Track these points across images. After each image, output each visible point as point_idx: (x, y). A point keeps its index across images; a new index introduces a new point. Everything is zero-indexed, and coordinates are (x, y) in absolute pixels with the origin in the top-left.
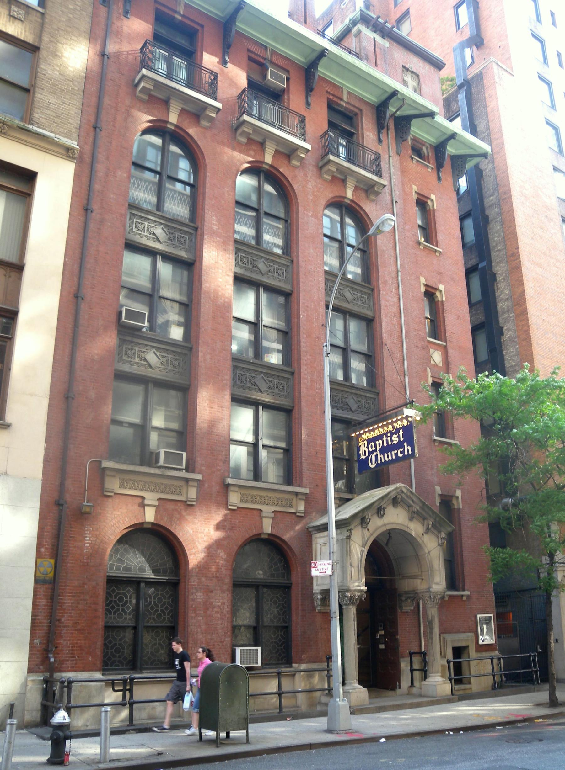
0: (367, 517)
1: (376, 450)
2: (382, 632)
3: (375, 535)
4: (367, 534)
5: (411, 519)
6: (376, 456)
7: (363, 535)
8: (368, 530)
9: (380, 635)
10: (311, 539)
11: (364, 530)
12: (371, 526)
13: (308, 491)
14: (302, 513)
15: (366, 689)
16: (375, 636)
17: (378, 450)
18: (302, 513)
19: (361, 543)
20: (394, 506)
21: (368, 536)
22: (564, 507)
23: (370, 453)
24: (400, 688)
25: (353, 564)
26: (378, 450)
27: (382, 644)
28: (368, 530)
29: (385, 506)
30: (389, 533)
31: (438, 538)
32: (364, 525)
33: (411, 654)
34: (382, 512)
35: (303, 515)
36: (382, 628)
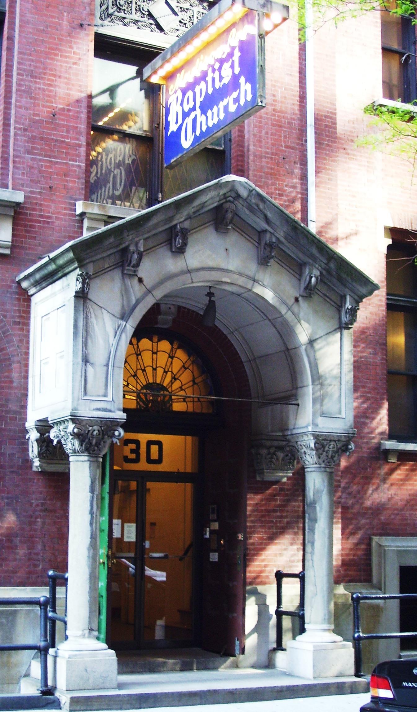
0: (132, 248)
1: (194, 109)
2: (215, 526)
3: (159, 294)
4: (136, 290)
5: (263, 262)
6: (195, 120)
7: (125, 292)
8: (140, 280)
9: (211, 532)
10: (29, 306)
11: (128, 282)
12: (149, 269)
13: (19, 197)
14: (6, 247)
15: (112, 652)
16: (203, 533)
17: (198, 105)
18: (6, 247)
19: (117, 310)
20: (217, 230)
21: (139, 295)
22: (118, 1)
23: (186, 115)
24: (243, 651)
25: (91, 359)
26: (198, 105)
27: (215, 551)
28: (140, 280)
29: (187, 225)
30: (210, 294)
31: (339, 312)
32: (129, 269)
33: (280, 576)
34: (179, 241)
35: (8, 252)
36: (215, 516)
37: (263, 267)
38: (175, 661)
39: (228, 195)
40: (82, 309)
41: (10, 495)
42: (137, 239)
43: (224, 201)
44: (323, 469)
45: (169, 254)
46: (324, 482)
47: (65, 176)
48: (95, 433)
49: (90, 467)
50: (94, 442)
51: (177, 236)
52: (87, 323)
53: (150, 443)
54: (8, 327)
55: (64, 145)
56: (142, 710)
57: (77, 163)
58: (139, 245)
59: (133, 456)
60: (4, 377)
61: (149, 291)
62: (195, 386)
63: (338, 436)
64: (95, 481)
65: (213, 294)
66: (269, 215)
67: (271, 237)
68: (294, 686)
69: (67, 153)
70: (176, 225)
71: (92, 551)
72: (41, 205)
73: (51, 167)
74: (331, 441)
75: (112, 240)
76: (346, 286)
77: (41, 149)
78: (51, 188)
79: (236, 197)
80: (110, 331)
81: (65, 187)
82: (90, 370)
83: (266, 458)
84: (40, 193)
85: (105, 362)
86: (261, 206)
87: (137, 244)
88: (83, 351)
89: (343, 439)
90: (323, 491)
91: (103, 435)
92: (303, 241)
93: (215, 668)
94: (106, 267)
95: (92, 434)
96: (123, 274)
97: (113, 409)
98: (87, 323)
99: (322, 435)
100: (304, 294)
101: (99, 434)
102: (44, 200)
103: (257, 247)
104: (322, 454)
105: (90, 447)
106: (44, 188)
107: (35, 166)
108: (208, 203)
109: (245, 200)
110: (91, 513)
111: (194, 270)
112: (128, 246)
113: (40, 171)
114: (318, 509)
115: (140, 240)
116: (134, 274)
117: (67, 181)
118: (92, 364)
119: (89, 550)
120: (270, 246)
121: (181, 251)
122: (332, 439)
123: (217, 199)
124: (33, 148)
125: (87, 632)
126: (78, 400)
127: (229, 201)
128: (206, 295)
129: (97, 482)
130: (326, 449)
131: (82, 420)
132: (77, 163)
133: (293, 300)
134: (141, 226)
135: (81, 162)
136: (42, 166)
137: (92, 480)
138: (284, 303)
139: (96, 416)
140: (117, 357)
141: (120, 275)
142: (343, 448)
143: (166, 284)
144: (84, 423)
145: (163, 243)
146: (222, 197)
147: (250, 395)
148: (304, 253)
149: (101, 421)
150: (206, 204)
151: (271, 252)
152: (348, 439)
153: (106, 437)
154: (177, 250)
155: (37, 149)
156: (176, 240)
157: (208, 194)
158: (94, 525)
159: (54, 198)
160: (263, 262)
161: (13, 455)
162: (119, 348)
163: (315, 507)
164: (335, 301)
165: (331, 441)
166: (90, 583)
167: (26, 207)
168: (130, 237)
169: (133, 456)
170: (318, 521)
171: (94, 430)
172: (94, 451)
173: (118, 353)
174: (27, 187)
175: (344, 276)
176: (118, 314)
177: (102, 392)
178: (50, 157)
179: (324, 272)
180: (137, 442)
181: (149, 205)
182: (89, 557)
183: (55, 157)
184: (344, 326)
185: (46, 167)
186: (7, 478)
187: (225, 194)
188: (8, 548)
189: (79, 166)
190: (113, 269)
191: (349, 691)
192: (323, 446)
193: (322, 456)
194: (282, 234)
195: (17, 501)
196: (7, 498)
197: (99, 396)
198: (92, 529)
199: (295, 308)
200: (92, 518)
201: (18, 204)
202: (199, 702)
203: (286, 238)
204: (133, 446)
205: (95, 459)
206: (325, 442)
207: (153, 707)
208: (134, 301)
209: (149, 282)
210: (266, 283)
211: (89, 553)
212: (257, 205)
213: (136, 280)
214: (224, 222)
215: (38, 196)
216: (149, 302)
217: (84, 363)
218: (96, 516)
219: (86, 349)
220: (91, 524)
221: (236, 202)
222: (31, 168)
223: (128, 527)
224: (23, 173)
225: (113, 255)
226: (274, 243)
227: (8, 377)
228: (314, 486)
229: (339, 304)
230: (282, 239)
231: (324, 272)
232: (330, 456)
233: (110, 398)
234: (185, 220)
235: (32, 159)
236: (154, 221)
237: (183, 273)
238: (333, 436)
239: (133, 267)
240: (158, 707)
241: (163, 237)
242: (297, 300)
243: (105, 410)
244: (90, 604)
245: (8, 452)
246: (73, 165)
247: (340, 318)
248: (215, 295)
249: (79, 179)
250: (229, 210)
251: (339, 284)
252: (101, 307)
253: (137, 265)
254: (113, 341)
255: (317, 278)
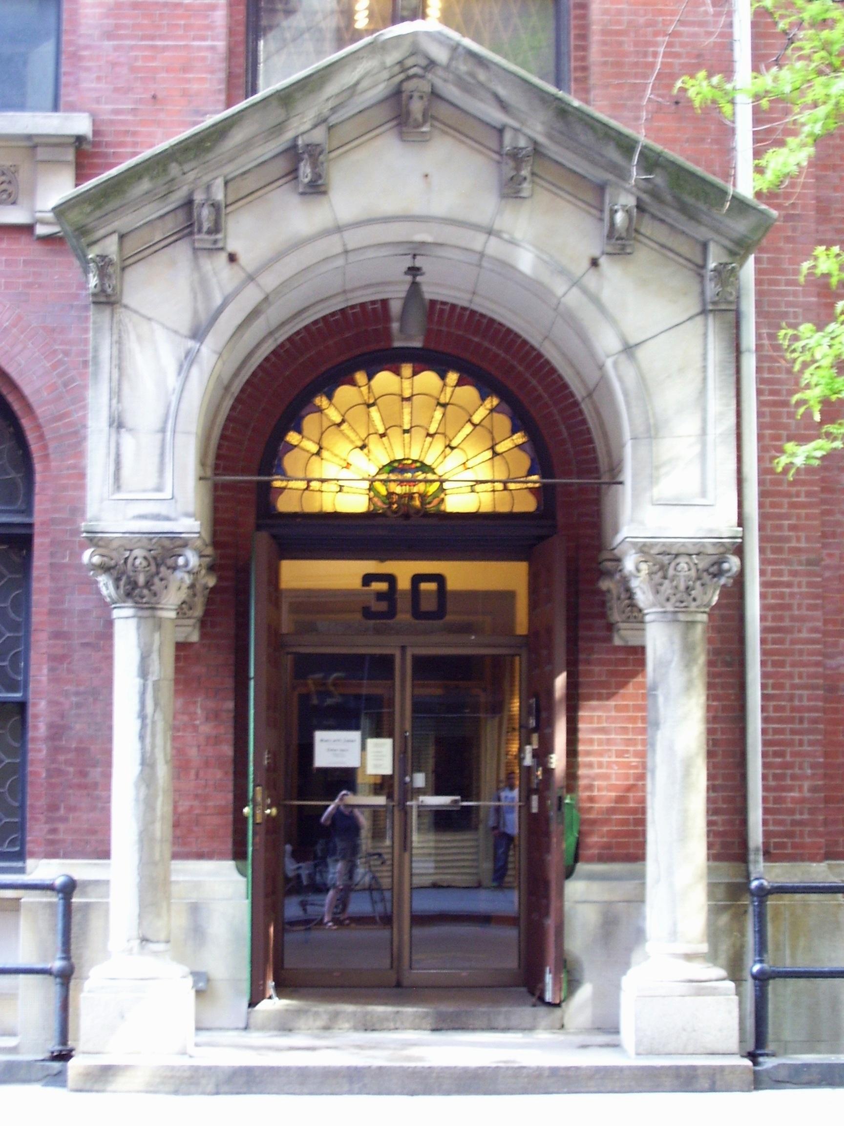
0: (199, 197)
3: (270, 281)
5: (511, 190)
7: (202, 286)
8: (232, 258)
12: (246, 234)
19: (184, 323)
20: (402, 137)
29: (319, 136)
32: (203, 239)
34: (306, 171)
37: (511, 201)
38: (425, 1010)
39: (410, 62)
40: (107, 326)
41: (82, 688)
42: (206, 179)
43: (402, 76)
44: (670, 616)
45: (294, 200)
46: (672, 643)
47: (185, 70)
48: (138, 562)
49: (138, 628)
50: (141, 579)
51: (302, 160)
52: (120, 351)
53: (417, 579)
54: (73, 373)
55: (180, 11)
56: (191, 1097)
57: (208, 43)
58: (214, 189)
59: (383, 606)
60: (68, 469)
61: (251, 278)
62: (497, 458)
63: (695, 544)
64: (149, 656)
65: (418, 269)
66: (502, 92)
67: (515, 139)
68: (568, 1069)
69: (187, 27)
70: (295, 138)
71: (143, 790)
72: (134, 134)
73: (153, 58)
74: (677, 555)
75: (145, 185)
76: (699, 222)
77: (135, 26)
78: (154, 97)
79: (428, 65)
80: (170, 364)
81: (185, 93)
82: (128, 441)
83: (619, 598)
84: (134, 111)
85: (158, 425)
86: (482, 76)
87: (208, 188)
88: (110, 407)
89: (711, 550)
90: (670, 662)
91: (158, 566)
92: (586, 138)
93: (531, 1029)
94: (157, 240)
95: (133, 565)
96: (195, 250)
97: (173, 515)
98: (120, 351)
99: (656, 544)
100: (609, 249)
101: (149, 565)
102: (144, 123)
103: (499, 163)
104: (661, 584)
105: (133, 589)
106: (141, 101)
107: (123, 60)
108: (364, 84)
109: (447, 68)
110: (142, 716)
111: (350, 225)
112: (191, 193)
113: (133, 69)
114: (661, 700)
115: (216, 178)
116: (215, 249)
117: (188, 81)
118: (130, 430)
119: (137, 787)
120: (516, 156)
121: (317, 188)
122: (682, 550)
123: (385, 75)
124: (118, 27)
125: (136, 943)
126: (102, 500)
127: (415, 76)
128: (406, 273)
129: (155, 656)
130: (671, 572)
131: (111, 540)
132: (208, 43)
133: (586, 263)
134: (208, 150)
135: (218, 40)
136: (136, 58)
137: (142, 655)
138: (562, 272)
139: (137, 530)
140: (181, 414)
141: (190, 253)
142: (712, 570)
143: (287, 259)
144: (115, 544)
145: (283, 177)
146: (397, 69)
147: (597, 470)
148: (593, 162)
149: (151, 539)
150: (360, 87)
151: (518, 169)
152: (722, 550)
153: (163, 569)
154: (308, 190)
155: (124, 27)
156: (304, 169)
157: (355, 68)
158: (148, 740)
159: (162, 116)
160: (511, 190)
161: (86, 612)
162: (185, 394)
163: (655, 696)
164: (689, 256)
165: (677, 555)
166: (141, 849)
167: (106, 142)
168: (191, 176)
169: (383, 606)
170: (662, 726)
171: (135, 558)
172: (142, 597)
173: (184, 406)
174: (106, 103)
175: (689, 200)
176: (185, 329)
177: (152, 482)
178: (153, 38)
179: (645, 197)
180: (390, 579)
181: (229, 105)
182: (137, 800)
183: (162, 37)
184: (710, 307)
185: (145, 58)
186: (76, 656)
187: (400, 63)
188: (81, 786)
189: (213, 48)
190: (176, 241)
191: (707, 1086)
192: (663, 568)
193: (663, 588)
194: (539, 128)
195: (95, 700)
196: (77, 694)
197: (145, 491)
198: (143, 748)
199: (591, 281)
200: (143, 726)
201: (80, 139)
202: (346, 1088)
203: (550, 137)
204: (383, 586)
205: (147, 613)
206: (666, 559)
207: (245, 1093)
208: (218, 300)
209: (248, 259)
210: (518, 235)
211: (138, 794)
212: (472, 75)
213: (223, 257)
214: (411, 120)
215: (130, 118)
216: (251, 297)
217: (113, 430)
218: (154, 722)
219: (119, 402)
220: (142, 737)
221: (429, 76)
222: (114, 64)
223: (376, 745)
224: (99, 79)
225: (172, 215)
226: (522, 149)
227: (75, 467)
228: (655, 653)
229: (699, 261)
230: (541, 139)
231: (645, 197)
232: (682, 587)
233: (167, 494)
234: (315, 126)
235: (116, 48)
236: (237, 137)
237: (326, 233)
238: (683, 545)
239: (210, 232)
240: (255, 1093)
241: (281, 166)
242: (594, 263)
243: (157, 517)
244: (140, 891)
245: (78, 606)
246: (200, 49)
247: (703, 293)
248: (424, 269)
249: (212, 72)
250: (416, 95)
251: (683, 218)
252: (149, 319)
253: (216, 228)
254: (172, 381)
255: (628, 212)
